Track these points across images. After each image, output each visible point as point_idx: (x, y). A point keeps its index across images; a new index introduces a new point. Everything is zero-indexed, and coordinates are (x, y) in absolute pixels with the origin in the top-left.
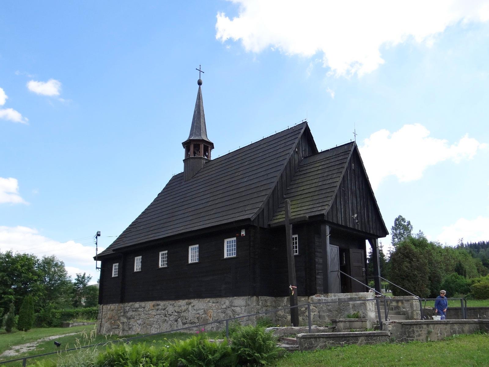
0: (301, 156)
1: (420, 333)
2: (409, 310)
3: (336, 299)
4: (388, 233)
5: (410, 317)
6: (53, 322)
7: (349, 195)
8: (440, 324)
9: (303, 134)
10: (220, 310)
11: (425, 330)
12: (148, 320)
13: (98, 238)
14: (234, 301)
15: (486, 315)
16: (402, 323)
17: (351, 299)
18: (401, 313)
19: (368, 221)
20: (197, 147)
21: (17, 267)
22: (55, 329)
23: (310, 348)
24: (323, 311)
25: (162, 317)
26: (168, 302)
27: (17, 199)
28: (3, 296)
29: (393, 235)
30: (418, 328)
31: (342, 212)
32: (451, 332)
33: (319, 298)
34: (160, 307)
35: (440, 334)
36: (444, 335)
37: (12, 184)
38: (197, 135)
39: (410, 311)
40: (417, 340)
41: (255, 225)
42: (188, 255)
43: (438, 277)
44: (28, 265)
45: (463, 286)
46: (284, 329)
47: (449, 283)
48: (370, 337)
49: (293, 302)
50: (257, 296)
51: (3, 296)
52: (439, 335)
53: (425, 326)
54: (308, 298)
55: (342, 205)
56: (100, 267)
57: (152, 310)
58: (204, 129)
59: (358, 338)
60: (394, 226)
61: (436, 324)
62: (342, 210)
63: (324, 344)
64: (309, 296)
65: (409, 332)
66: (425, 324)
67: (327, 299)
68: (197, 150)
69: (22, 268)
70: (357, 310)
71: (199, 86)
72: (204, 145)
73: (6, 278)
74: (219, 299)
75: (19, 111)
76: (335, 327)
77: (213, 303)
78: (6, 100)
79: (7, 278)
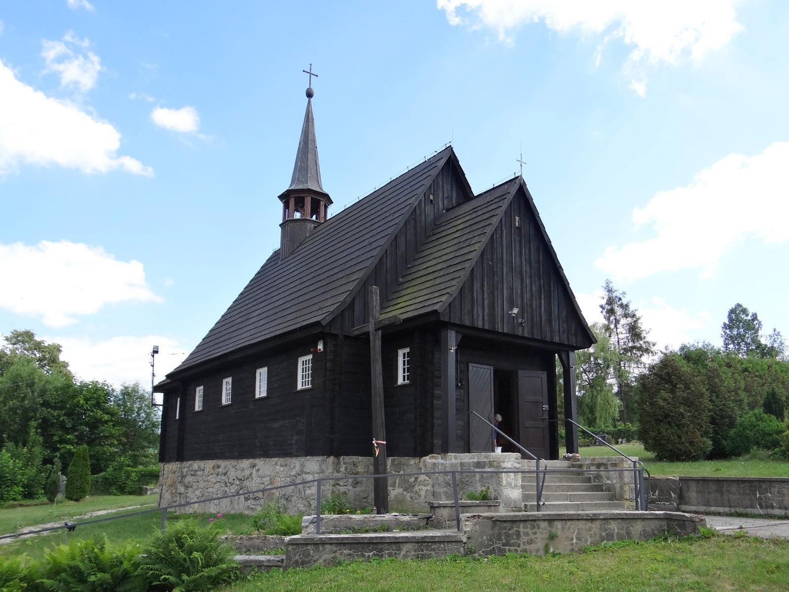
0: (441, 207)
1: (533, 537)
2: (616, 483)
3: (458, 463)
4: (593, 340)
5: (618, 495)
6: (126, 486)
7: (505, 274)
8: (579, 520)
9: (449, 167)
10: (288, 479)
11: (545, 531)
12: (207, 490)
13: (155, 357)
14: (306, 465)
15: (771, 493)
16: (492, 518)
17: (478, 464)
18: (604, 488)
19: (550, 321)
20: (303, 199)
21: (78, 402)
22: (131, 497)
23: (303, 563)
24: (439, 485)
25: (222, 487)
26: (229, 463)
27: (145, 295)
28: (58, 446)
29: (726, 339)
30: (527, 528)
31: (486, 305)
32: (601, 536)
33: (434, 461)
34: (220, 470)
35: (578, 539)
36: (587, 540)
37: (135, 270)
38: (302, 183)
39: (618, 485)
40: (525, 551)
41: (335, 332)
42: (255, 384)
43: (730, 417)
44: (96, 398)
45: (769, 435)
46: (335, 518)
47: (745, 428)
48: (424, 544)
49: (378, 467)
50: (337, 455)
51: (58, 446)
52: (575, 541)
53: (544, 525)
54: (420, 460)
55: (485, 293)
56: (162, 404)
57: (212, 474)
58: (313, 171)
59: (401, 546)
60: (727, 323)
61: (569, 520)
62: (486, 302)
63: (333, 555)
64: (421, 457)
65: (508, 536)
66: (544, 520)
67: (445, 462)
68: (301, 207)
69: (87, 403)
70: (487, 485)
71: (308, 99)
72: (312, 198)
73: (63, 420)
74: (289, 460)
75: (138, 159)
76: (431, 517)
77: (281, 466)
78: (120, 140)
79: (64, 417)
